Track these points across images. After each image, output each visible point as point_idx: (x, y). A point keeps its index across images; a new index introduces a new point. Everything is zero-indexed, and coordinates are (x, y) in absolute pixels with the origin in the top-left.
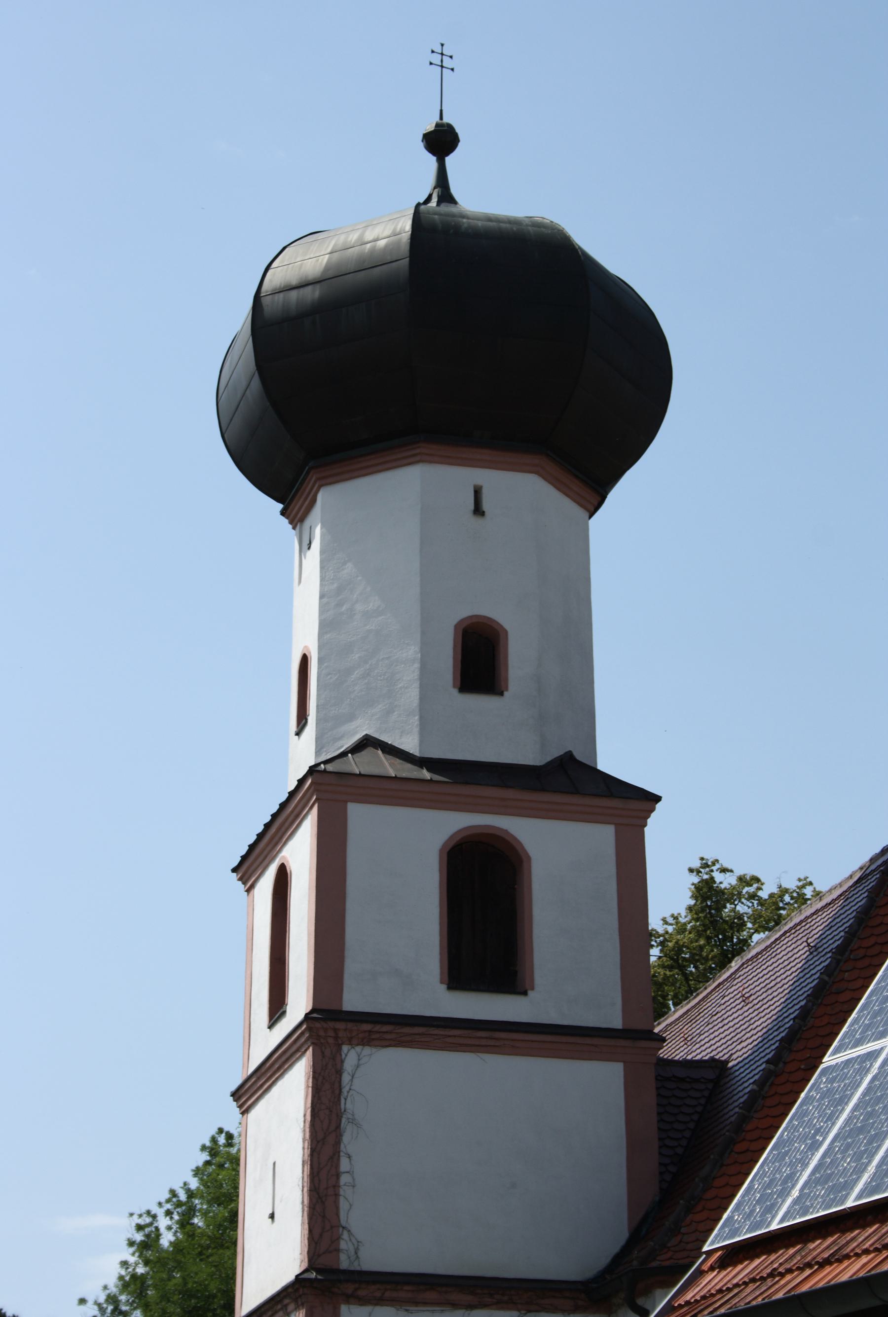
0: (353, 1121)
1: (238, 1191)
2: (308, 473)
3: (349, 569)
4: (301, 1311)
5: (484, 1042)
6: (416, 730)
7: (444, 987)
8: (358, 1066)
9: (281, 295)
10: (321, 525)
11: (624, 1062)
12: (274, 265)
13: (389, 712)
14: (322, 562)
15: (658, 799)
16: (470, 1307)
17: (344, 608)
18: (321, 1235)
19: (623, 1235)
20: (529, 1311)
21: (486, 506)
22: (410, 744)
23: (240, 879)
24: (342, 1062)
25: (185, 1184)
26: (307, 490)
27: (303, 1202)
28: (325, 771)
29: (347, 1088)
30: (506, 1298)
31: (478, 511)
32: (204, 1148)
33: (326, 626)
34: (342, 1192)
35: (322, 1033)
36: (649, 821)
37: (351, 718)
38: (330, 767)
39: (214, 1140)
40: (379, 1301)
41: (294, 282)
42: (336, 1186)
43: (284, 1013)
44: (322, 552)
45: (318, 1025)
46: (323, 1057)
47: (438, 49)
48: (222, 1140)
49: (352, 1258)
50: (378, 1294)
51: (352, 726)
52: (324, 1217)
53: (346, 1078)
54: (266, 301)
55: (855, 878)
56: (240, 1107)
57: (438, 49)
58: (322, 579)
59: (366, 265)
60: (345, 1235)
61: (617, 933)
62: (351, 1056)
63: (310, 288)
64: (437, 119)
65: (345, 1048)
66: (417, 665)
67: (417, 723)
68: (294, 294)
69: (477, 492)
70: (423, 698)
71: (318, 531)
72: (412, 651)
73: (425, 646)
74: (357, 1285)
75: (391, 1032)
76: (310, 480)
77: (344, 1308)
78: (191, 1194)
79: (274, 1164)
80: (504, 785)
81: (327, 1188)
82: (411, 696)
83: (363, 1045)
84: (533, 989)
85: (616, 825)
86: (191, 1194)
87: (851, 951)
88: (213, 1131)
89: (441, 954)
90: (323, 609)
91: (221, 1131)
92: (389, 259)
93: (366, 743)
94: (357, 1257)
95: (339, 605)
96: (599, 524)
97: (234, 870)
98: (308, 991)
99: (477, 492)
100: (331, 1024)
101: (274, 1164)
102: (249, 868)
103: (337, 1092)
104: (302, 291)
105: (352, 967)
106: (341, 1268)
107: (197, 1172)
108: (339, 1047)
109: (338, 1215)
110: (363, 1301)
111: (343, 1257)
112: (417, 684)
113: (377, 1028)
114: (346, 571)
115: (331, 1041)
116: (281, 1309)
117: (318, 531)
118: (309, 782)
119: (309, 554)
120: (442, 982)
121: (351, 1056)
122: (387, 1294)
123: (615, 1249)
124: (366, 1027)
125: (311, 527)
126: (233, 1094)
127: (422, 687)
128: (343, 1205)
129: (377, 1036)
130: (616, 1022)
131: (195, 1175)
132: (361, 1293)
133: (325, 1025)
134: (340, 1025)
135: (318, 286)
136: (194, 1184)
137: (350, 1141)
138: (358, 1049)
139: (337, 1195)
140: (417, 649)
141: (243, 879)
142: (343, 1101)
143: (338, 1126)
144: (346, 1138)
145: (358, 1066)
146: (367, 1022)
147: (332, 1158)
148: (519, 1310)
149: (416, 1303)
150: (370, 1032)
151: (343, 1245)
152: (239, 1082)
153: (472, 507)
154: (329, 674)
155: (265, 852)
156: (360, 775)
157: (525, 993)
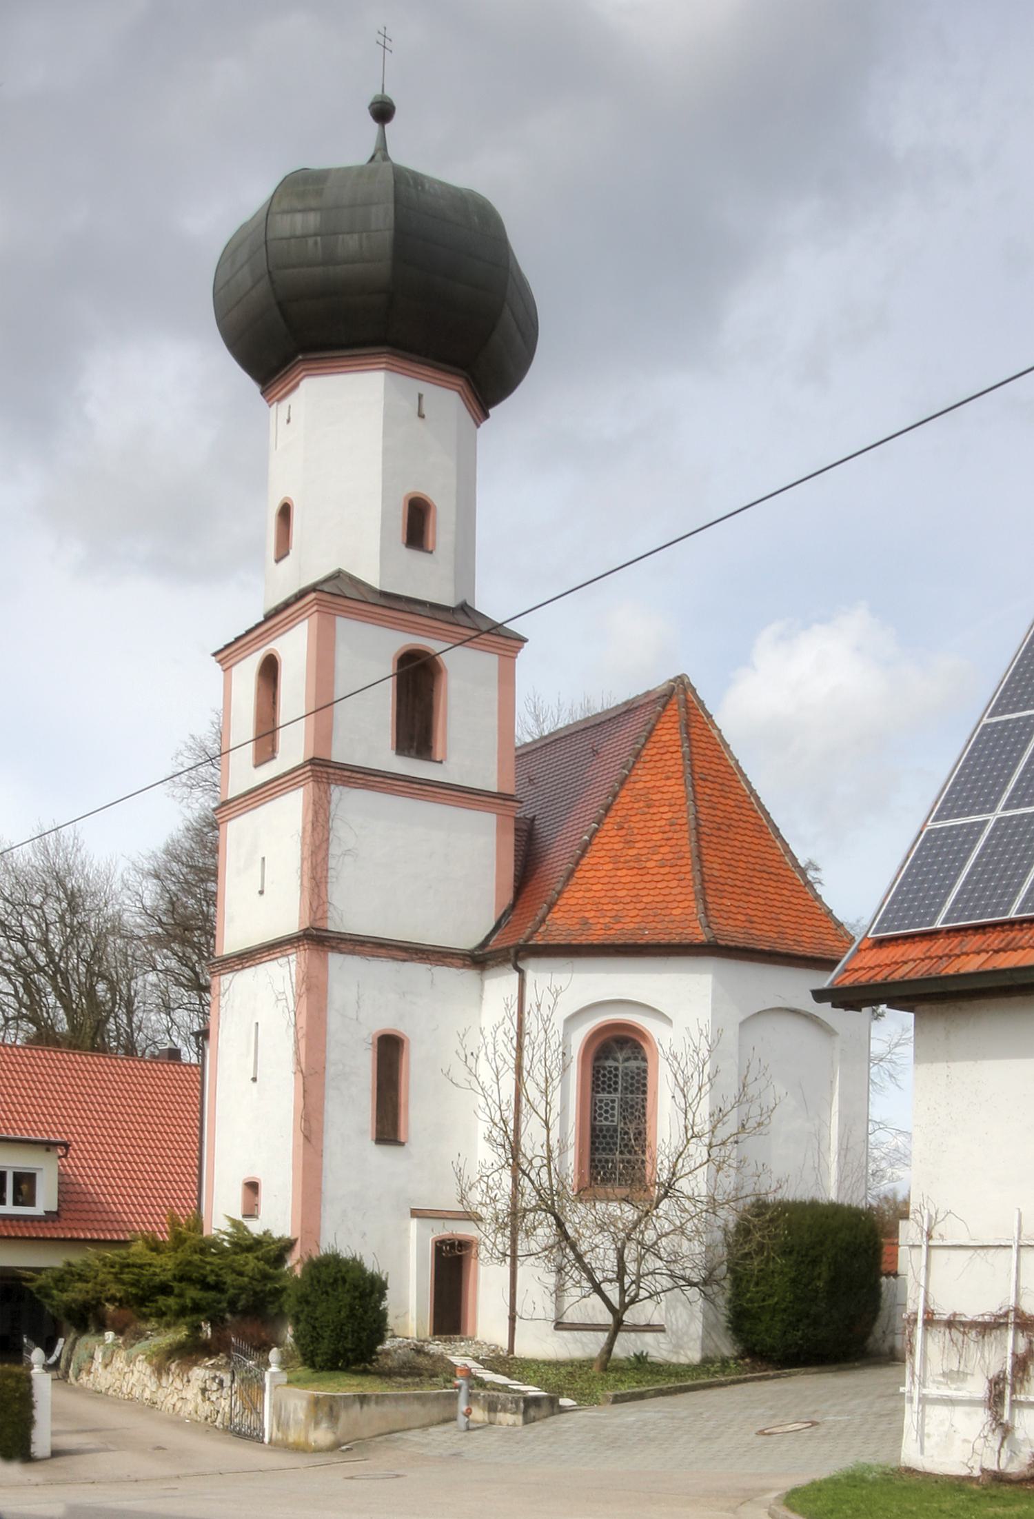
1: (211, 886)
4: (293, 957)
8: (340, 799)
21: (425, 411)
27: (302, 884)
36: (519, 655)
40: (352, 953)
42: (326, 877)
47: (382, 31)
53: (333, 806)
57: (382, 31)
61: (496, 729)
62: (337, 792)
64: (380, 93)
96: (479, 430)
97: (215, 654)
113: (354, 775)
130: (495, 790)
138: (341, 787)
139: (327, 882)
143: (328, 839)
145: (340, 799)
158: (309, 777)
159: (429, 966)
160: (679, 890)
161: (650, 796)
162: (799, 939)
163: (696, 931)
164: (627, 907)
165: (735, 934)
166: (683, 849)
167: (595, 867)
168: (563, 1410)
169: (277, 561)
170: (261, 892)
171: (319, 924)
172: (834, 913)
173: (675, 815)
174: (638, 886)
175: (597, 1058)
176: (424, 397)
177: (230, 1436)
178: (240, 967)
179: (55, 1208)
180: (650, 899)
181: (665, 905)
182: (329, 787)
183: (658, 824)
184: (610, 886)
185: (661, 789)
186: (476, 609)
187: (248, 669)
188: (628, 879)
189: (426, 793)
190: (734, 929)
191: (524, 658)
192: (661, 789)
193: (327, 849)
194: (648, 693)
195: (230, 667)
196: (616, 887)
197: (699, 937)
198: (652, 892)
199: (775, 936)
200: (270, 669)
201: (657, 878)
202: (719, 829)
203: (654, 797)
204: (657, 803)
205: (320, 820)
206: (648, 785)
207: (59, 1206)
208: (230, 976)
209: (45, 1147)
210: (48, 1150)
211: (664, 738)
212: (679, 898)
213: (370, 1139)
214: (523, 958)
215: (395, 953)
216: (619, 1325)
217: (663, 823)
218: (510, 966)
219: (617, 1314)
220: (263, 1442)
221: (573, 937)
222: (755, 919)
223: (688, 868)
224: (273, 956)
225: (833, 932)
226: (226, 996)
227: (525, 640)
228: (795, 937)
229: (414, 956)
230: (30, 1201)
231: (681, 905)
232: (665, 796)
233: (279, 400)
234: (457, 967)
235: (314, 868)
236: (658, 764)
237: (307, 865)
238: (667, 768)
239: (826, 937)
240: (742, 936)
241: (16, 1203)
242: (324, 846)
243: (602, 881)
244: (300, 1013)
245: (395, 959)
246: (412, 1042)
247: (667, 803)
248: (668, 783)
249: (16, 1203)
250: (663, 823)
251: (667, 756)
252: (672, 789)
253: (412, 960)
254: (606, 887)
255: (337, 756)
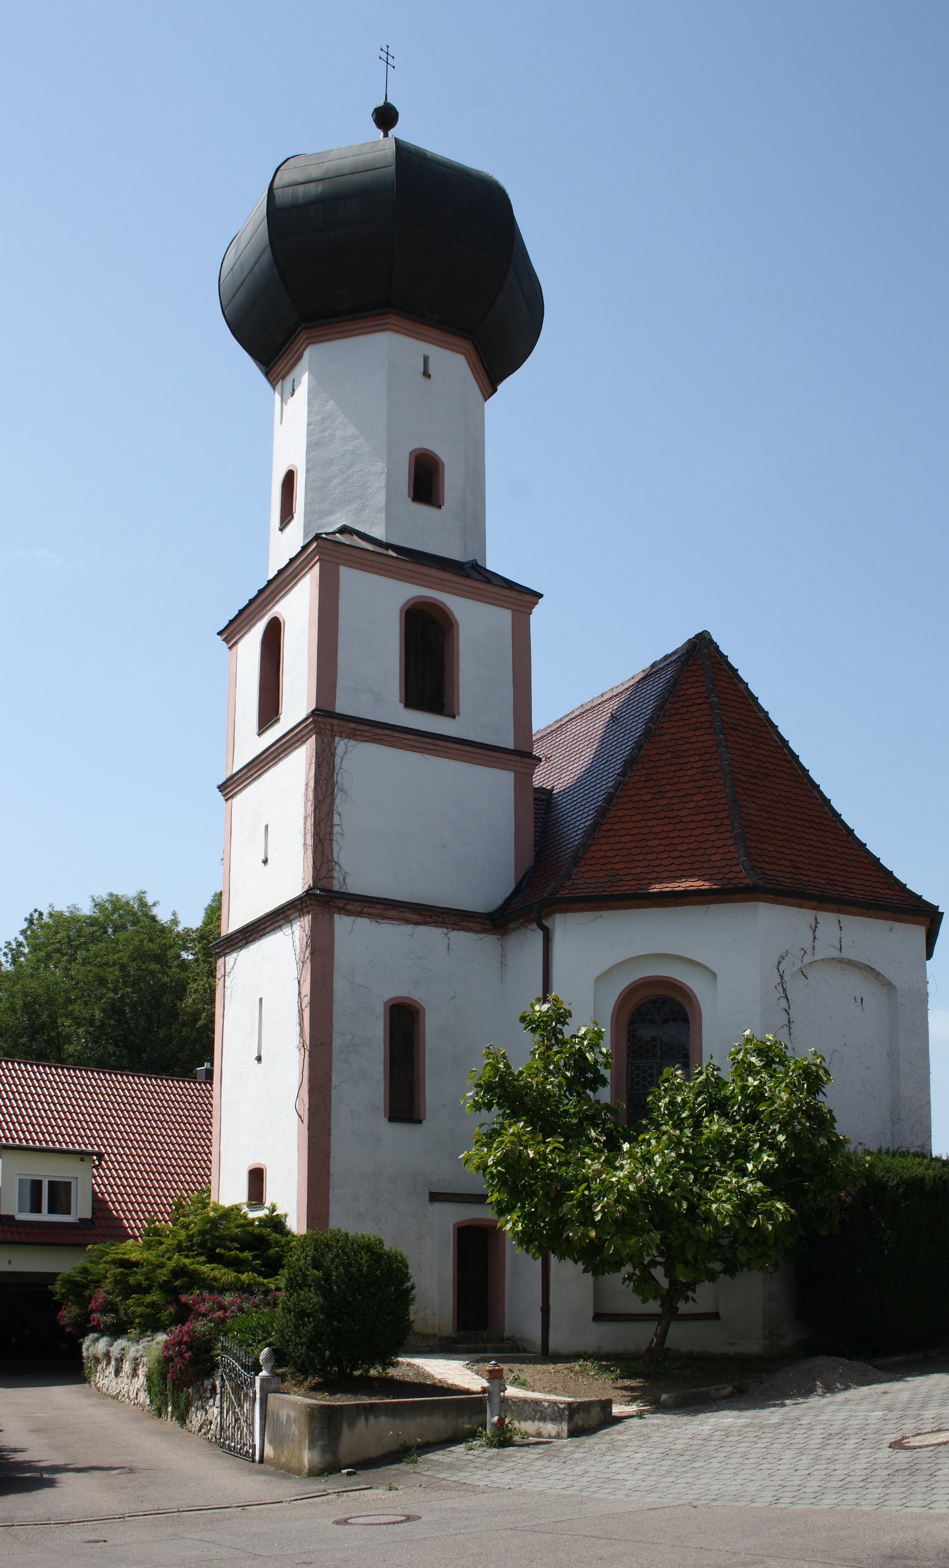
0: (342, 790)
2: (300, 332)
3: (331, 405)
5: (428, 746)
6: (383, 523)
7: (402, 705)
8: (346, 752)
9: (291, 188)
10: (310, 373)
11: (515, 772)
12: (282, 168)
13: (362, 509)
14: (309, 399)
15: (540, 596)
16: (417, 923)
17: (327, 433)
18: (321, 866)
19: (511, 886)
20: (454, 930)
21: (431, 371)
22: (378, 532)
23: (224, 640)
24: (335, 748)
25: (16, 938)
26: (295, 349)
28: (326, 539)
29: (338, 767)
30: (440, 919)
31: (426, 374)
32: (26, 919)
33: (312, 446)
34: (334, 838)
35: (322, 726)
37: (331, 512)
38: (329, 537)
39: (31, 915)
40: (360, 914)
41: (301, 180)
42: (331, 834)
43: (279, 719)
44: (309, 392)
45: (320, 719)
46: (323, 743)
47: (385, 49)
48: (36, 915)
49: (342, 884)
50: (359, 909)
51: (332, 518)
52: (323, 853)
53: (337, 760)
54: (277, 193)
55: (637, 679)
56: (224, 796)
57: (385, 49)
58: (309, 412)
59: (359, 169)
60: (337, 868)
62: (341, 745)
63: (313, 184)
65: (337, 739)
66: (384, 477)
67: (384, 517)
68: (301, 189)
69: (426, 360)
70: (388, 501)
71: (305, 378)
72: (380, 466)
73: (390, 464)
74: (346, 902)
75: (368, 731)
76: (299, 340)
77: (336, 917)
78: (20, 945)
79: (267, 827)
80: (444, 570)
81: (325, 835)
82: (380, 499)
83: (349, 738)
84: (459, 715)
85: (513, 610)
86: (20, 945)
87: (666, 710)
88: (32, 911)
89: (400, 682)
90: (310, 434)
91: (36, 910)
92: (378, 165)
93: (344, 530)
94: (345, 883)
95: (323, 431)
97: (220, 633)
98: (309, 696)
99: (426, 360)
100: (329, 720)
101: (267, 827)
102: (232, 632)
103: (332, 769)
104: (307, 186)
105: (342, 683)
106: (335, 889)
107: (23, 932)
108: (333, 737)
109: (332, 853)
110: (349, 913)
111: (335, 882)
112: (384, 491)
113: (360, 727)
114: (327, 407)
115: (328, 732)
116: (283, 918)
117: (305, 378)
118: (315, 545)
119: (291, 401)
120: (400, 702)
121: (341, 745)
122: (365, 910)
123: (507, 895)
124: (352, 725)
125: (294, 380)
126: (219, 787)
127: (387, 492)
128: (335, 847)
129: (359, 733)
130: (510, 745)
131: (21, 934)
132: (349, 907)
133: (325, 721)
134: (335, 722)
135: (320, 183)
136: (21, 939)
137: (340, 803)
138: (346, 740)
139: (331, 840)
140: (385, 465)
141: (227, 640)
142: (335, 775)
143: (332, 793)
144: (338, 801)
145: (346, 752)
146: (353, 722)
147: (328, 814)
148: (447, 928)
149: (384, 918)
150: (355, 729)
151: (336, 874)
152: (224, 779)
153: (422, 370)
154: (314, 481)
155: (254, 614)
156: (350, 546)
157: (454, 717)
158: (312, 730)
159: (445, 930)
160: (717, 836)
161: (678, 747)
162: (848, 886)
163: (739, 875)
164: (660, 856)
165: (782, 879)
166: (718, 795)
167: (622, 819)
168: (619, 1420)
169: (281, 530)
170: (265, 862)
171: (324, 883)
172: (881, 861)
173: (707, 764)
174: (671, 835)
175: (632, 1022)
176: (431, 360)
177: (219, 1451)
178: (244, 942)
179: (89, 1215)
180: (685, 847)
181: (702, 852)
182: (333, 740)
183: (689, 773)
184: (641, 837)
185: (689, 740)
186: (489, 567)
187: (252, 641)
188: (659, 829)
189: (437, 748)
190: (779, 874)
191: (538, 617)
192: (689, 740)
193: (332, 804)
194: (666, 657)
195: (236, 643)
196: (646, 837)
197: (743, 881)
198: (686, 840)
199: (824, 882)
200: (273, 634)
201: (690, 826)
202: (755, 777)
203: (683, 748)
204: (686, 754)
205: (324, 773)
206: (676, 737)
207: (93, 1213)
208: (234, 955)
209: (79, 1157)
210: (82, 1160)
211: (688, 692)
212: (718, 844)
213: (382, 1114)
214: (548, 915)
215: (408, 915)
216: (669, 1314)
217: (694, 771)
218: (534, 926)
219: (670, 1299)
220: (254, 1461)
221: (601, 889)
222: (800, 865)
223: (725, 814)
224: (277, 925)
225: (883, 881)
226: (231, 975)
227: (541, 596)
228: (844, 884)
229: (429, 919)
230: (68, 1212)
231: (720, 851)
232: (694, 746)
233: (283, 378)
234: (475, 931)
235: (317, 824)
236: (685, 717)
237: (310, 821)
238: (694, 720)
239: (876, 885)
240: (789, 881)
241: (51, 1211)
242: (328, 801)
243: (631, 832)
244: (304, 981)
245: (408, 922)
246: (427, 1010)
247: (697, 752)
248: (696, 733)
249: (51, 1211)
250: (694, 771)
251: (695, 708)
252: (701, 739)
253: (426, 924)
254: (636, 838)
255: (342, 707)
